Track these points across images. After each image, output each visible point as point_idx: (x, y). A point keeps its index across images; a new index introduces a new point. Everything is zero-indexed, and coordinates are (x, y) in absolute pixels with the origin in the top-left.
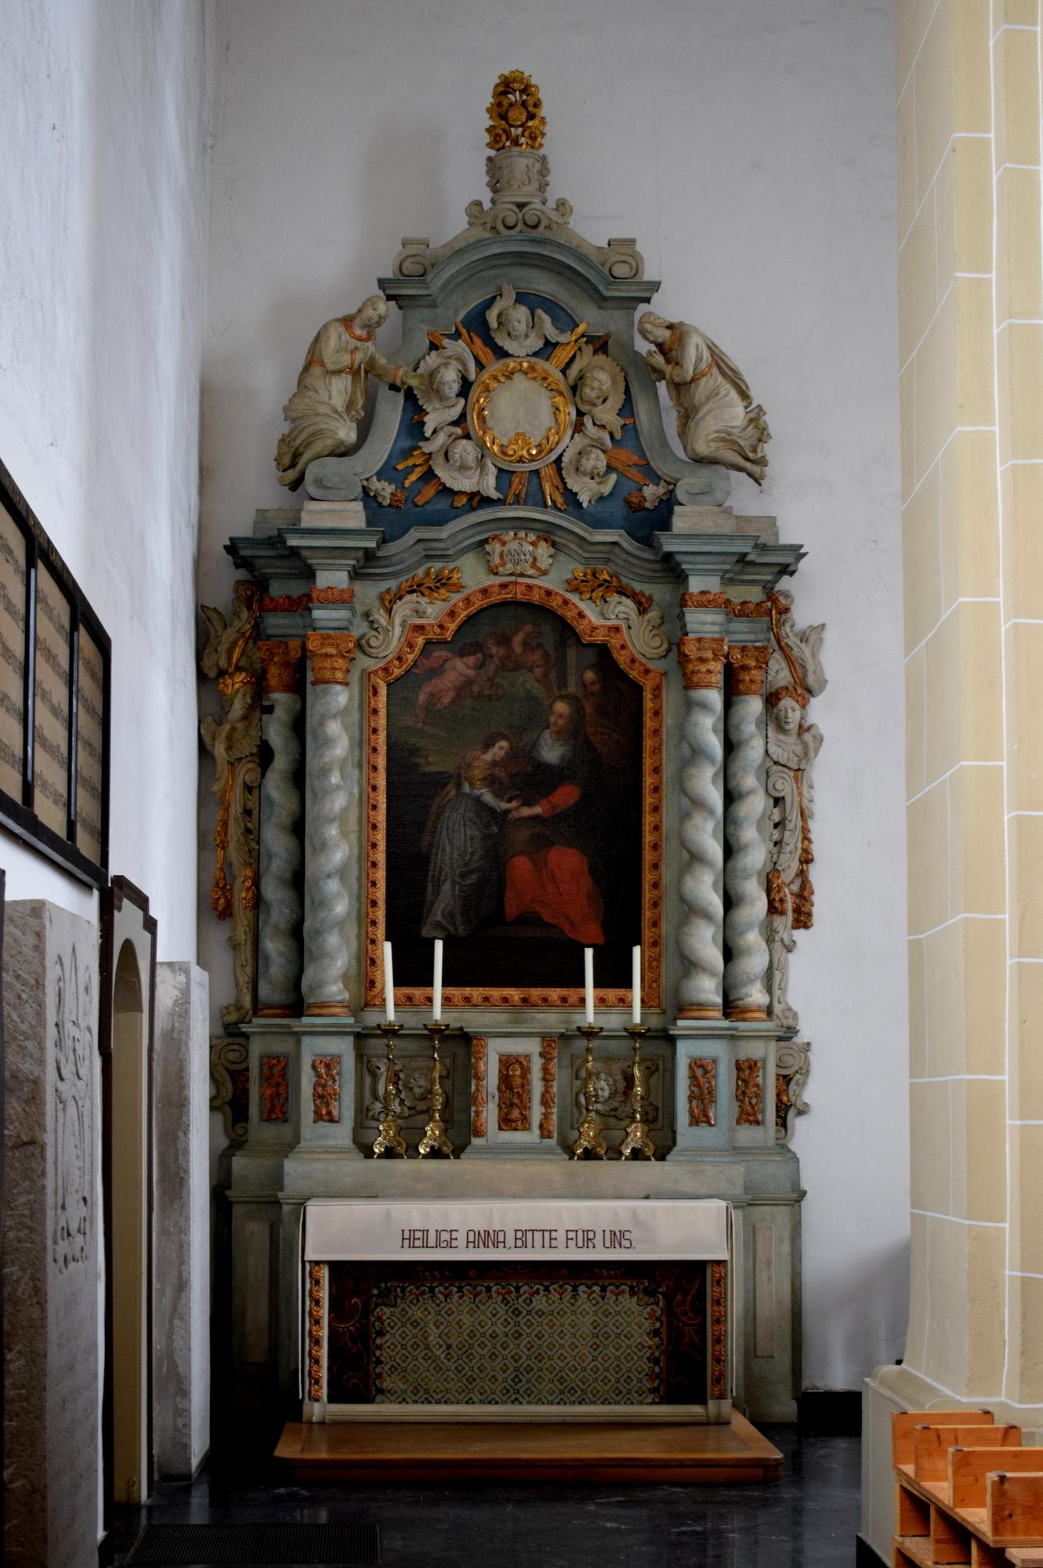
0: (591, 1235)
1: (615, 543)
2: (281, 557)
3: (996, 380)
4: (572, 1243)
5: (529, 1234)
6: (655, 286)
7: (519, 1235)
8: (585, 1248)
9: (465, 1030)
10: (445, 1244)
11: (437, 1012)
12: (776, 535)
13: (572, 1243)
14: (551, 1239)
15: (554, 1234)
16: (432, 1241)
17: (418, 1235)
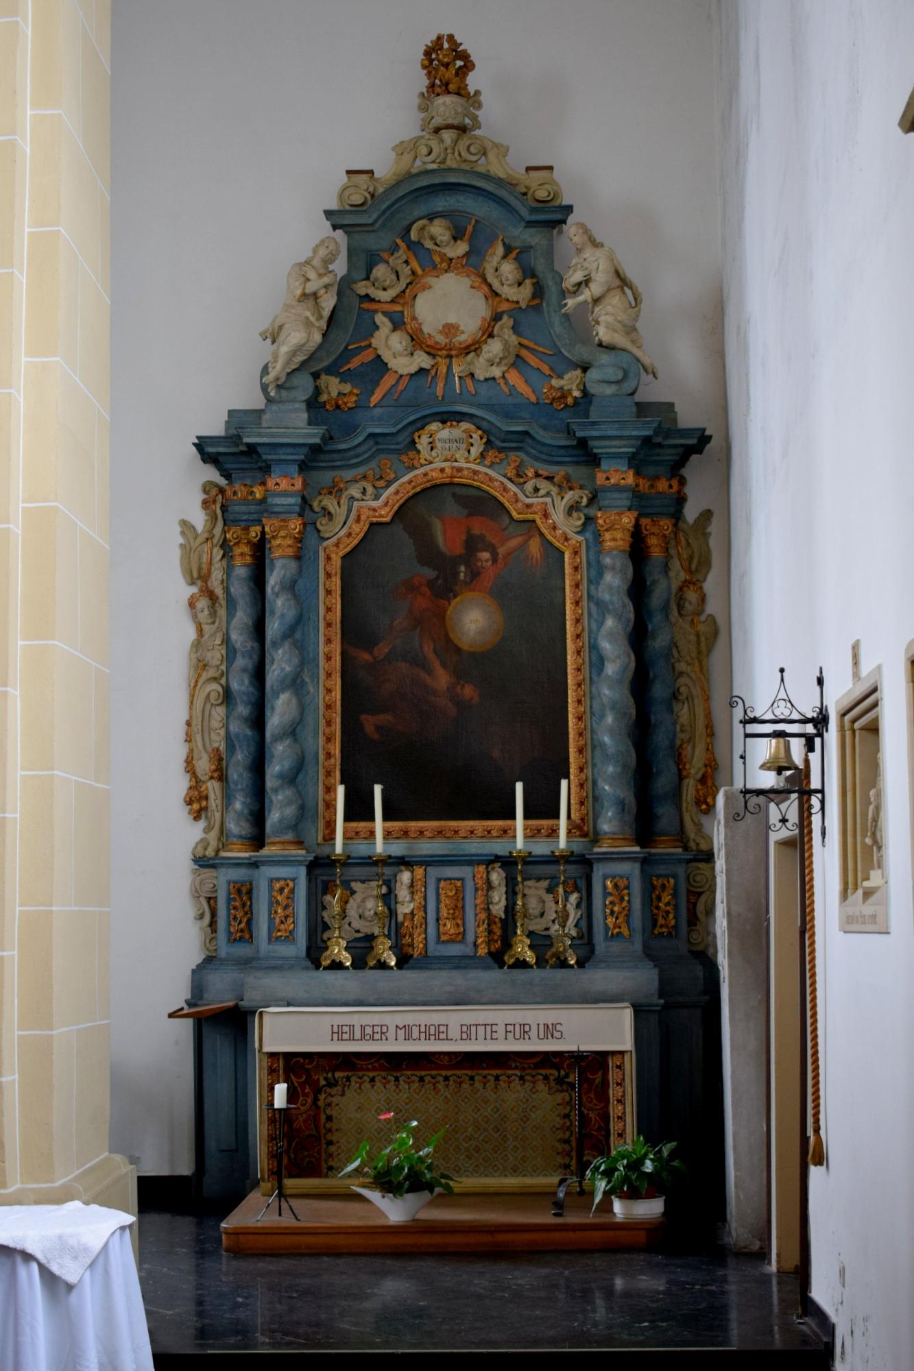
0: (527, 1028)
1: (526, 433)
2: (242, 453)
3: (22, 411)
4: (510, 1036)
5: (473, 1028)
6: (569, 209)
7: (465, 1029)
8: (522, 1039)
9: (587, 857)
10: (368, 1037)
11: (520, 843)
12: (675, 420)
13: (510, 1036)
14: (492, 1032)
15: (495, 1028)
16: (358, 1035)
17: (346, 1029)
